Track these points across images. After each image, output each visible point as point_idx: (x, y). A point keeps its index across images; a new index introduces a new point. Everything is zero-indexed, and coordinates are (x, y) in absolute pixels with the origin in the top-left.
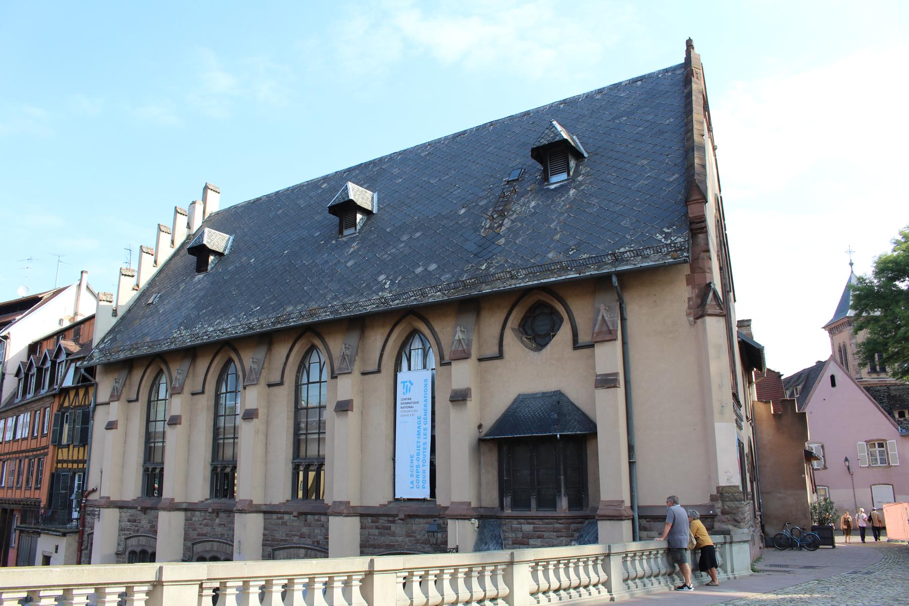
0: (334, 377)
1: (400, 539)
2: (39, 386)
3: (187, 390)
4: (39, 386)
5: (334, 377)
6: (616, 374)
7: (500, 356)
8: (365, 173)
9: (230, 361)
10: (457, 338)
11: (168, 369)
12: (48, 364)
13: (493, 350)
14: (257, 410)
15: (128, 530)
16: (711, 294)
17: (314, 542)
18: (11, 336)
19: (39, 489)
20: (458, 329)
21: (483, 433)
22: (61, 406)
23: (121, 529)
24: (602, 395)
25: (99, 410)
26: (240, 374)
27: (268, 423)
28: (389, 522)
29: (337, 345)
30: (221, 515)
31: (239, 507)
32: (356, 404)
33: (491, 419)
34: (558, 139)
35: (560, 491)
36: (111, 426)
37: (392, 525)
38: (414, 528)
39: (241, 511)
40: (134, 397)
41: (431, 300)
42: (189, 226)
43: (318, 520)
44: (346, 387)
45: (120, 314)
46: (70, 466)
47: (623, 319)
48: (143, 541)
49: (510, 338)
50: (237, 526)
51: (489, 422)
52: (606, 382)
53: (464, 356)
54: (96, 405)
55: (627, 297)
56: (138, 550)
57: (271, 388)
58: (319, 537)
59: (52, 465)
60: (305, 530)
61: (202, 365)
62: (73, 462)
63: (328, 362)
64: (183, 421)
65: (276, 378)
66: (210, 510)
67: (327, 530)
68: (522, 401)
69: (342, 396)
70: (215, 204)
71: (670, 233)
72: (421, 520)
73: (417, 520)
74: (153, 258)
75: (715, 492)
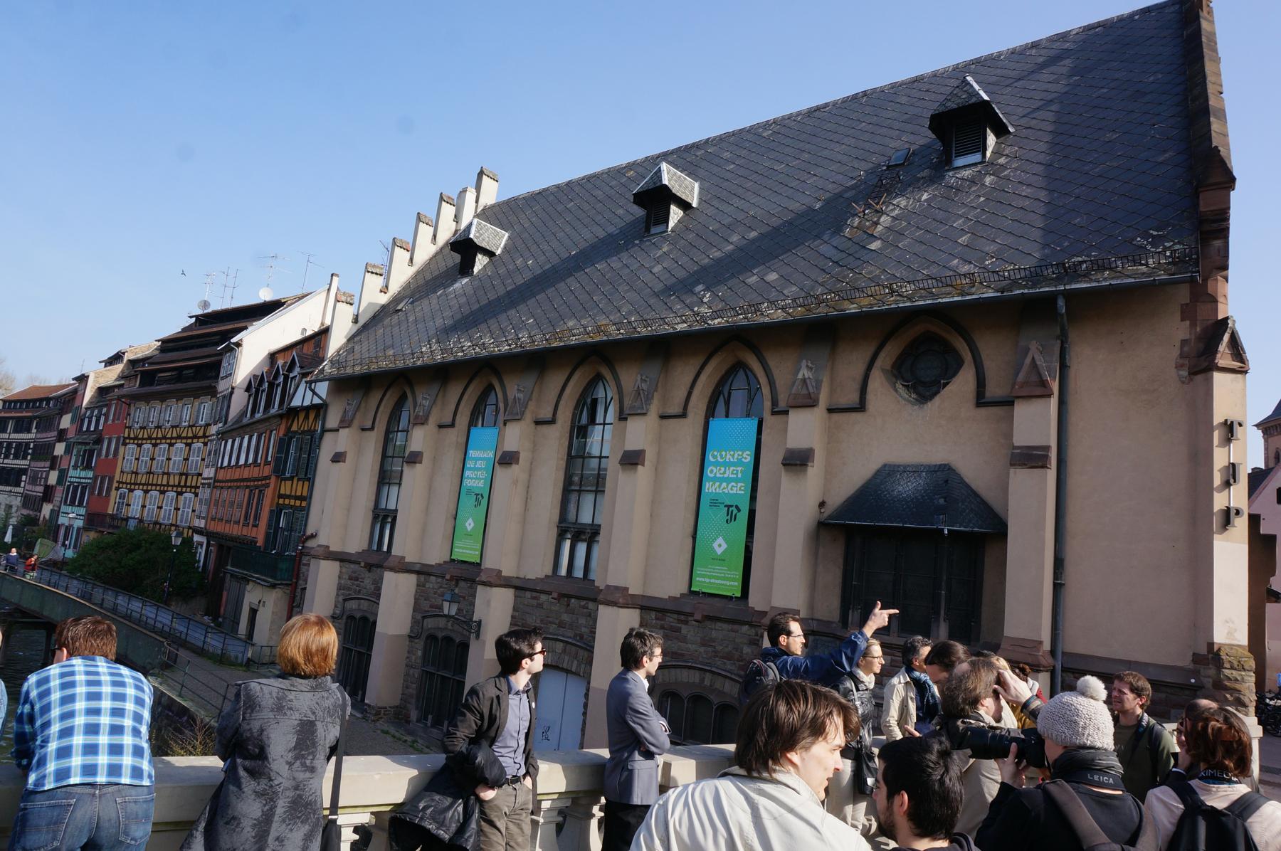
0: (622, 417)
1: (692, 647)
2: (268, 405)
3: (433, 420)
4: (268, 405)
5: (622, 417)
6: (1047, 448)
7: (861, 407)
8: (685, 157)
9: (490, 388)
10: (800, 376)
11: (413, 393)
12: (281, 379)
13: (851, 398)
14: (517, 453)
15: (349, 589)
16: (1226, 337)
17: (576, 635)
18: (244, 344)
19: (256, 526)
20: (804, 363)
21: (826, 515)
22: (288, 429)
23: (340, 588)
24: (1021, 479)
25: (328, 436)
26: (501, 405)
27: (531, 474)
28: (680, 621)
29: (631, 377)
30: (462, 584)
31: (483, 577)
32: (649, 457)
33: (841, 492)
34: (974, 100)
35: (938, 614)
36: (338, 458)
37: (683, 626)
38: (714, 634)
39: (485, 584)
40: (369, 425)
41: (767, 320)
42: (457, 218)
43: (584, 607)
44: (639, 433)
45: (362, 321)
46: (292, 502)
47: (1064, 367)
48: (364, 605)
49: (878, 382)
50: (478, 602)
51: (838, 497)
52: (1031, 458)
53: (809, 402)
54: (324, 431)
55: (1073, 335)
56: (358, 615)
57: (539, 427)
58: (584, 629)
59: (273, 499)
60: (565, 617)
61: (454, 391)
62: (296, 498)
63: (616, 397)
64: (425, 460)
65: (546, 413)
66: (448, 577)
67: (595, 621)
68: (889, 475)
69: (631, 445)
70: (491, 193)
71: (1164, 236)
72: (725, 626)
73: (719, 624)
74: (408, 255)
75: (1203, 650)
